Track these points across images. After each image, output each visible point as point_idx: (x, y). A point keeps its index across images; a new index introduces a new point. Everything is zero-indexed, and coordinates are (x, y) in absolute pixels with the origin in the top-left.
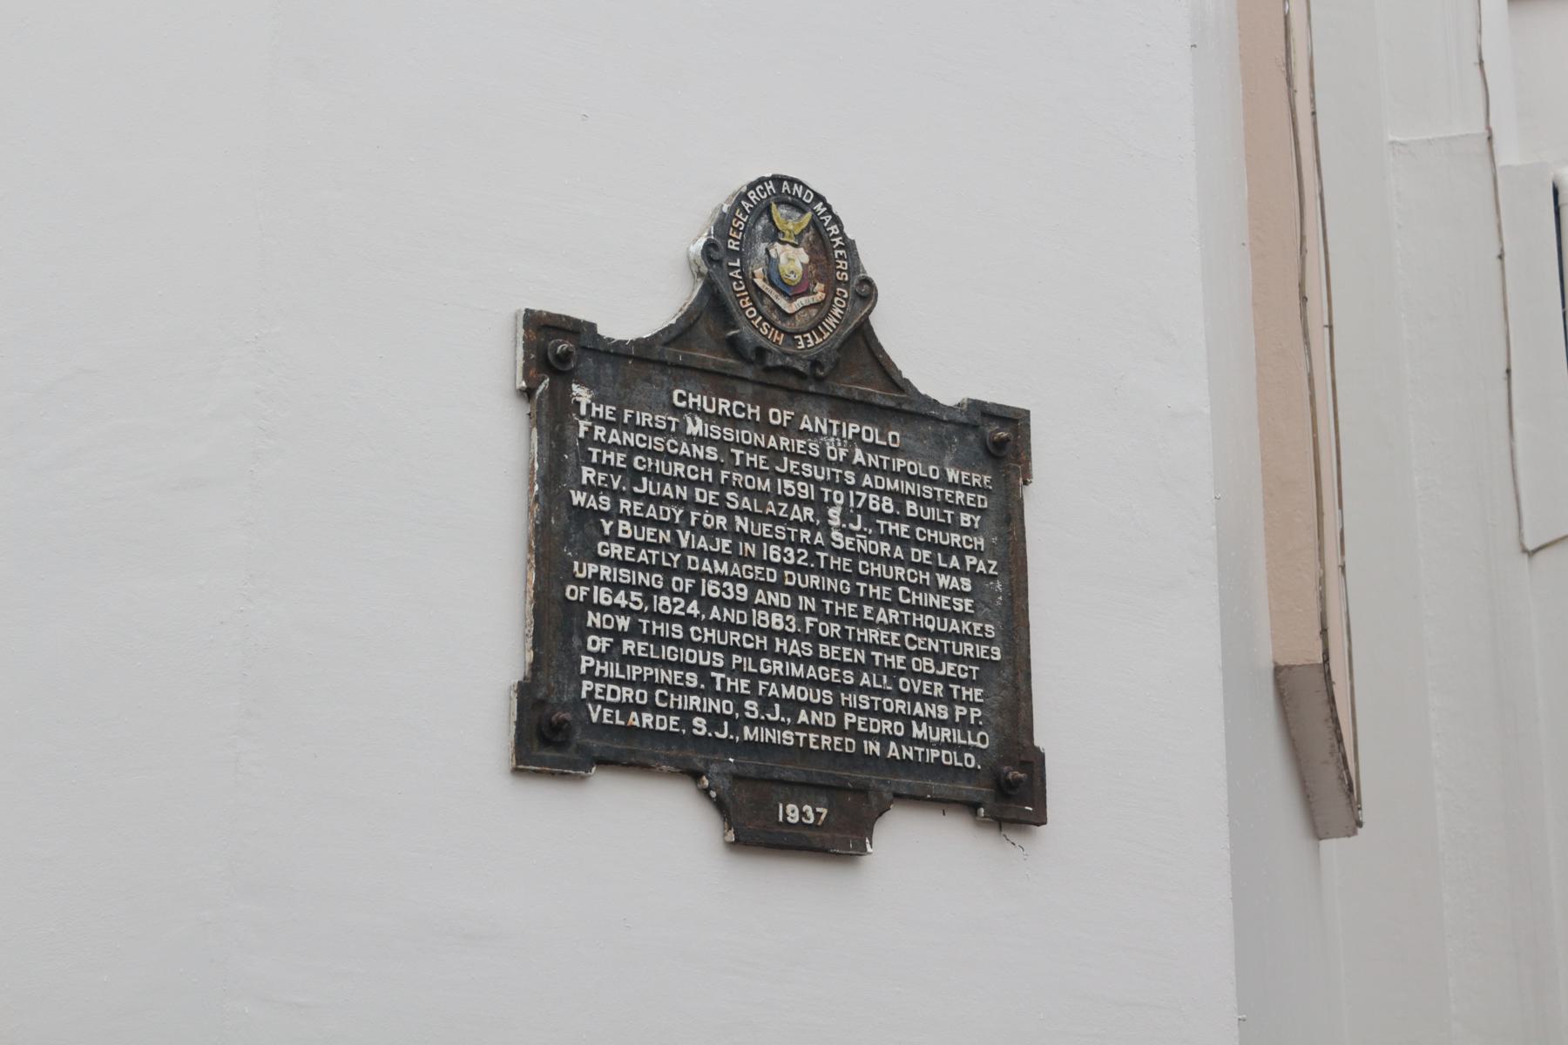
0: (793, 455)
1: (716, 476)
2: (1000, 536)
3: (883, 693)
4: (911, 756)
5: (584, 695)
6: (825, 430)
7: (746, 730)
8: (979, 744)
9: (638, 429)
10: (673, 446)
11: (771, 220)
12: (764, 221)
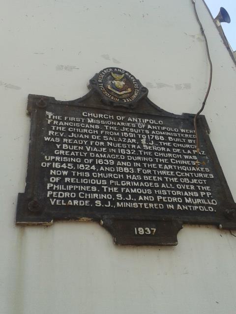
5: (48, 196)
6: (136, 121)
7: (118, 204)
8: (213, 204)
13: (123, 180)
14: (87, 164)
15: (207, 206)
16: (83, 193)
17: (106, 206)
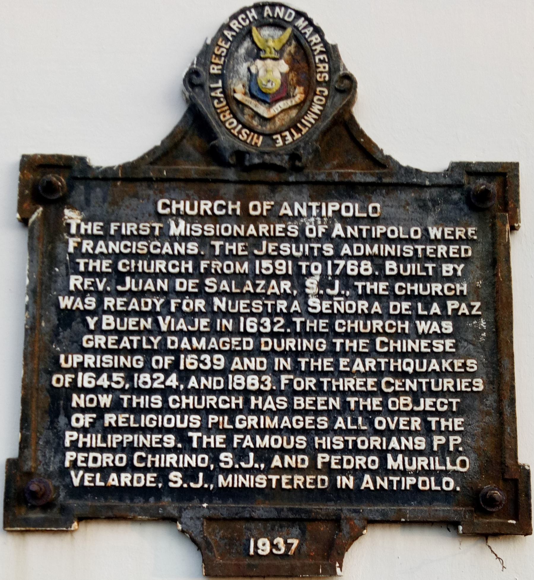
0: (272, 238)
1: (196, 267)
2: (485, 279)
3: (358, 432)
4: (386, 486)
5: (67, 464)
6: (304, 212)
7: (221, 478)
8: (458, 468)
9: (124, 237)
10: (156, 247)
11: (253, 42)
12: (247, 44)
13: (241, 412)
14: (158, 371)
15: (439, 475)
16: (144, 455)
17: (192, 485)
